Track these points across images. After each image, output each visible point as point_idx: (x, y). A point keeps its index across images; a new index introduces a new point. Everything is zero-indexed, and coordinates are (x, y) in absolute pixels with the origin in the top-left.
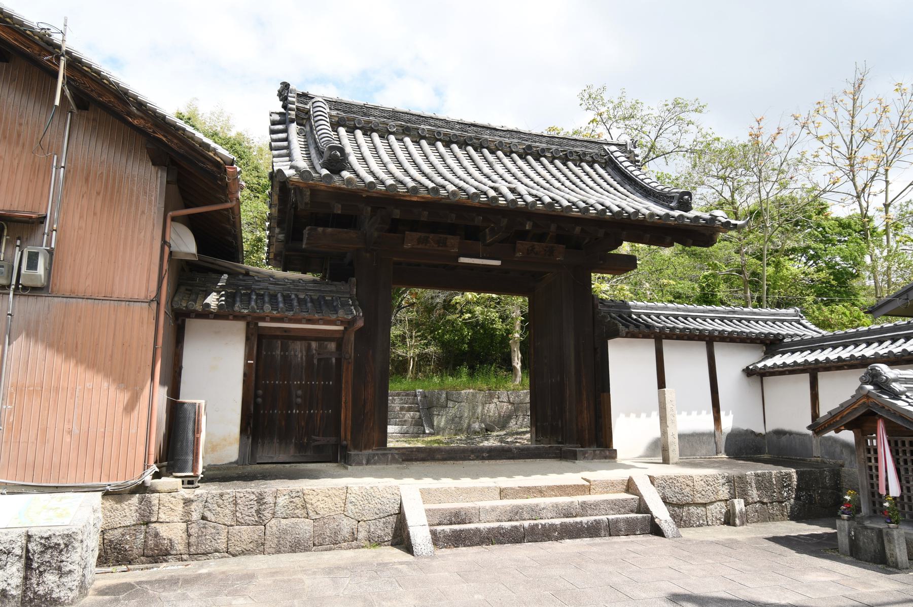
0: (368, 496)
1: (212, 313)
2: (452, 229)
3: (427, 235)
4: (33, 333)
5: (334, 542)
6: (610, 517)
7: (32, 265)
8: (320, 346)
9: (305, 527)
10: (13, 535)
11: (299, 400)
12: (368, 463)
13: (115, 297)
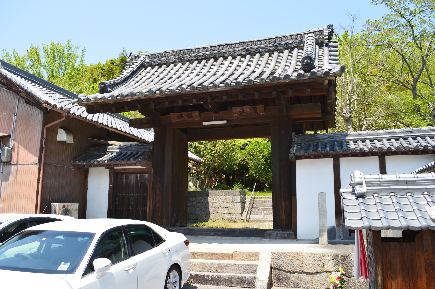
1: (430, 150)
2: (194, 108)
3: (181, 113)
8: (141, 176)
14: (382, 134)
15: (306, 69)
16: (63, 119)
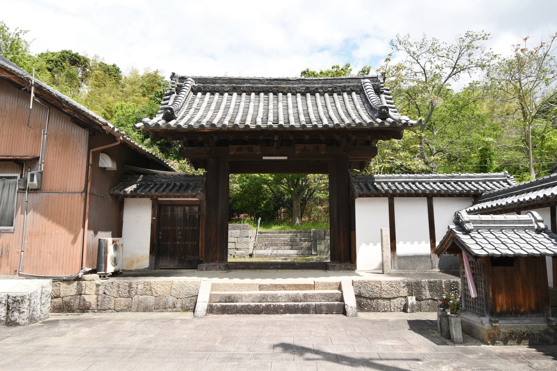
0: (182, 286)
4: (35, 209)
5: (165, 308)
6: (317, 303)
7: (32, 180)
8: (190, 209)
9: (151, 300)
10: (2, 296)
11: (180, 237)
12: (206, 270)
13: (68, 191)
14: (429, 178)
15: (382, 117)
16: (117, 144)
